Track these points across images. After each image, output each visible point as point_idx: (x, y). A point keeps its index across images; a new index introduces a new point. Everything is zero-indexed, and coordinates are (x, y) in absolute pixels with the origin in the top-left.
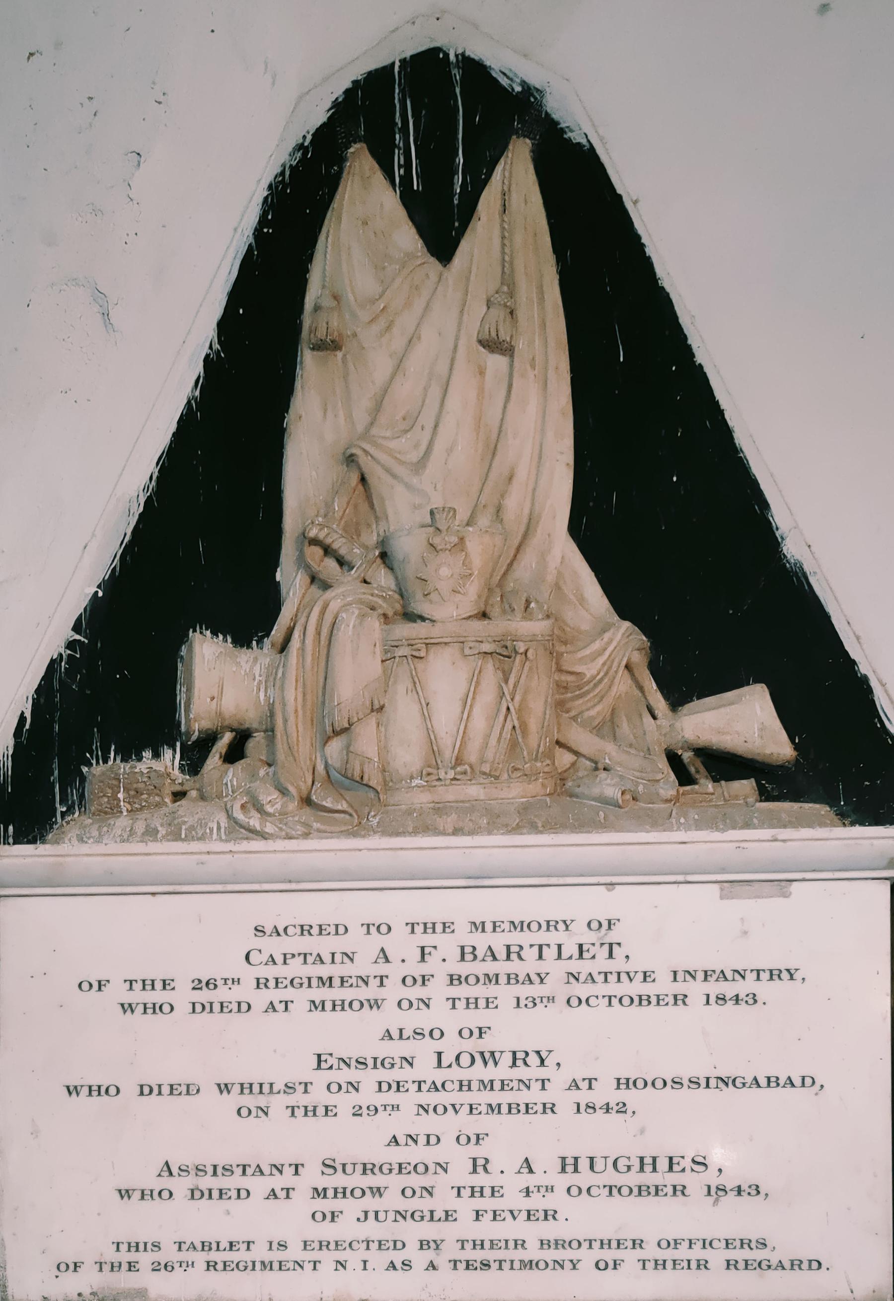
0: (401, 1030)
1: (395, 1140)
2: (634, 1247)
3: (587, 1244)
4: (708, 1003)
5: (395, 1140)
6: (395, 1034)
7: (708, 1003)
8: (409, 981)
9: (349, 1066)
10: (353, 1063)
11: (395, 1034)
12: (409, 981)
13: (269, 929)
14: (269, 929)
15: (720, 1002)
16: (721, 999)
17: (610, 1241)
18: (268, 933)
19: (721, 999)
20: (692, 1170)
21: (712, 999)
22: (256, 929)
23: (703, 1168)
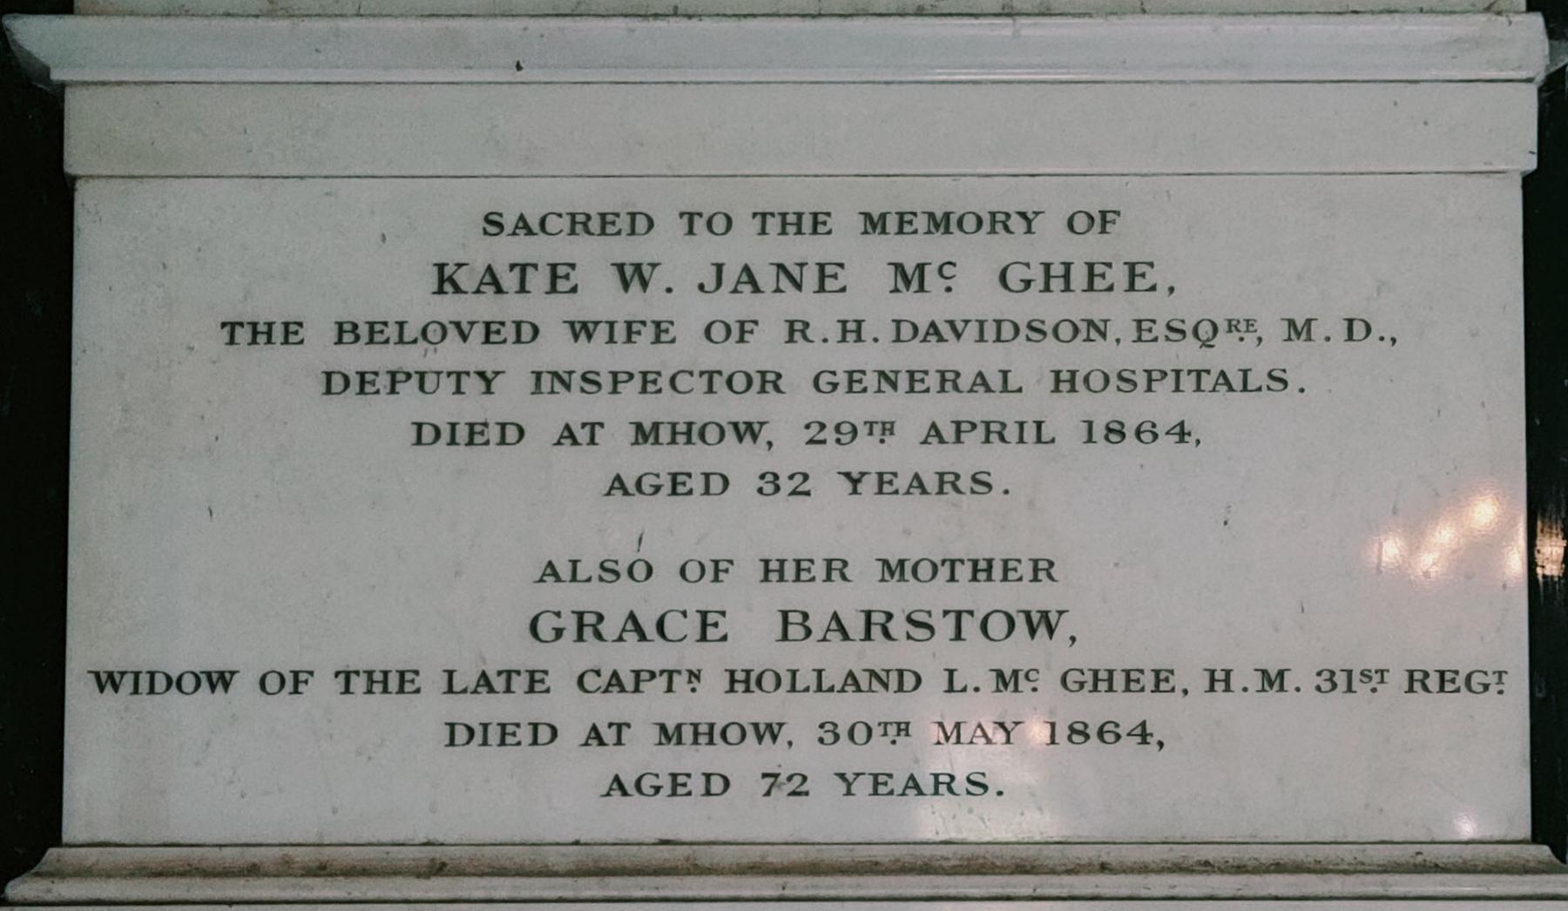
0: (575, 563)
1: (551, 570)
2: (1035, 579)
3: (944, 572)
4: (1090, 440)
5: (551, 570)
6: (564, 571)
7: (1090, 440)
8: (718, 332)
9: (568, 387)
10: (576, 381)
11: (564, 571)
12: (718, 332)
13: (509, 221)
14: (509, 221)
15: (1113, 437)
16: (1115, 432)
17: (696, 742)
18: (509, 228)
19: (1115, 432)
20: (909, 637)
21: (1099, 431)
22: (487, 220)
23: (927, 633)
